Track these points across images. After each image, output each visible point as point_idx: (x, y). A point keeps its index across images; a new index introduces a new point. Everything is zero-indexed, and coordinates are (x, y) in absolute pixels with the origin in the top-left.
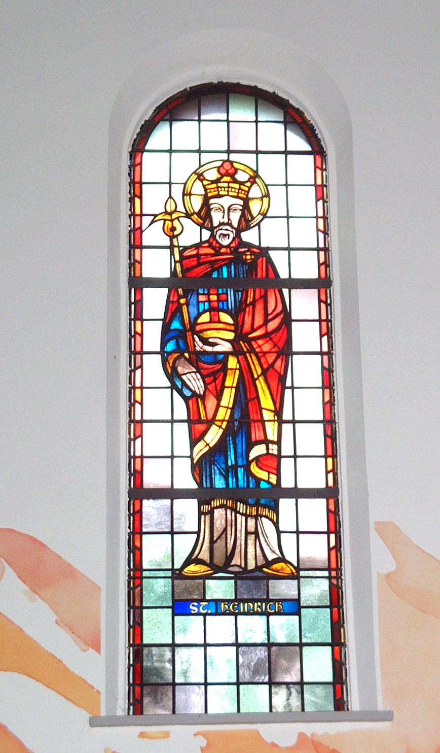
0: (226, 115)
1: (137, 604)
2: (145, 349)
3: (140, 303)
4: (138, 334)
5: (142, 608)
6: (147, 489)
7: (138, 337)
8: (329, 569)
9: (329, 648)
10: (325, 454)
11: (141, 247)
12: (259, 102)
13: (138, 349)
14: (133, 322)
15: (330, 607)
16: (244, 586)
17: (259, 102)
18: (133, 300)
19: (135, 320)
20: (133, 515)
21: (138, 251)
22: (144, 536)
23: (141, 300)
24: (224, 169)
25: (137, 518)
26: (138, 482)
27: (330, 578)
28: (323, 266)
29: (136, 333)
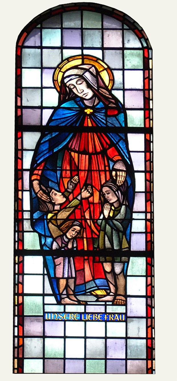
0: (80, 22)
1: (21, 356)
2: (25, 292)
3: (20, 77)
4: (19, 158)
5: (147, 359)
6: (25, 126)
7: (20, 285)
8: (146, 212)
9: (143, 154)
10: (145, 170)
11: (23, 295)
12: (104, 16)
13: (20, 292)
14: (17, 276)
15: (146, 276)
16: (88, 117)
17: (104, 16)
18: (17, 272)
19: (19, 274)
20: (18, 264)
21: (21, 298)
22: (25, 276)
23: (23, 345)
24: (77, 308)
25: (20, 351)
26: (21, 238)
27: (146, 220)
28: (149, 162)
29: (19, 282)
